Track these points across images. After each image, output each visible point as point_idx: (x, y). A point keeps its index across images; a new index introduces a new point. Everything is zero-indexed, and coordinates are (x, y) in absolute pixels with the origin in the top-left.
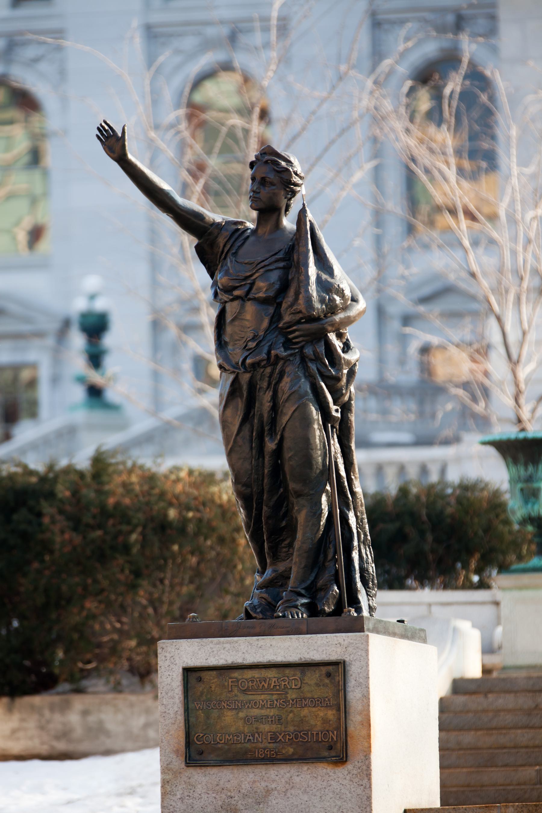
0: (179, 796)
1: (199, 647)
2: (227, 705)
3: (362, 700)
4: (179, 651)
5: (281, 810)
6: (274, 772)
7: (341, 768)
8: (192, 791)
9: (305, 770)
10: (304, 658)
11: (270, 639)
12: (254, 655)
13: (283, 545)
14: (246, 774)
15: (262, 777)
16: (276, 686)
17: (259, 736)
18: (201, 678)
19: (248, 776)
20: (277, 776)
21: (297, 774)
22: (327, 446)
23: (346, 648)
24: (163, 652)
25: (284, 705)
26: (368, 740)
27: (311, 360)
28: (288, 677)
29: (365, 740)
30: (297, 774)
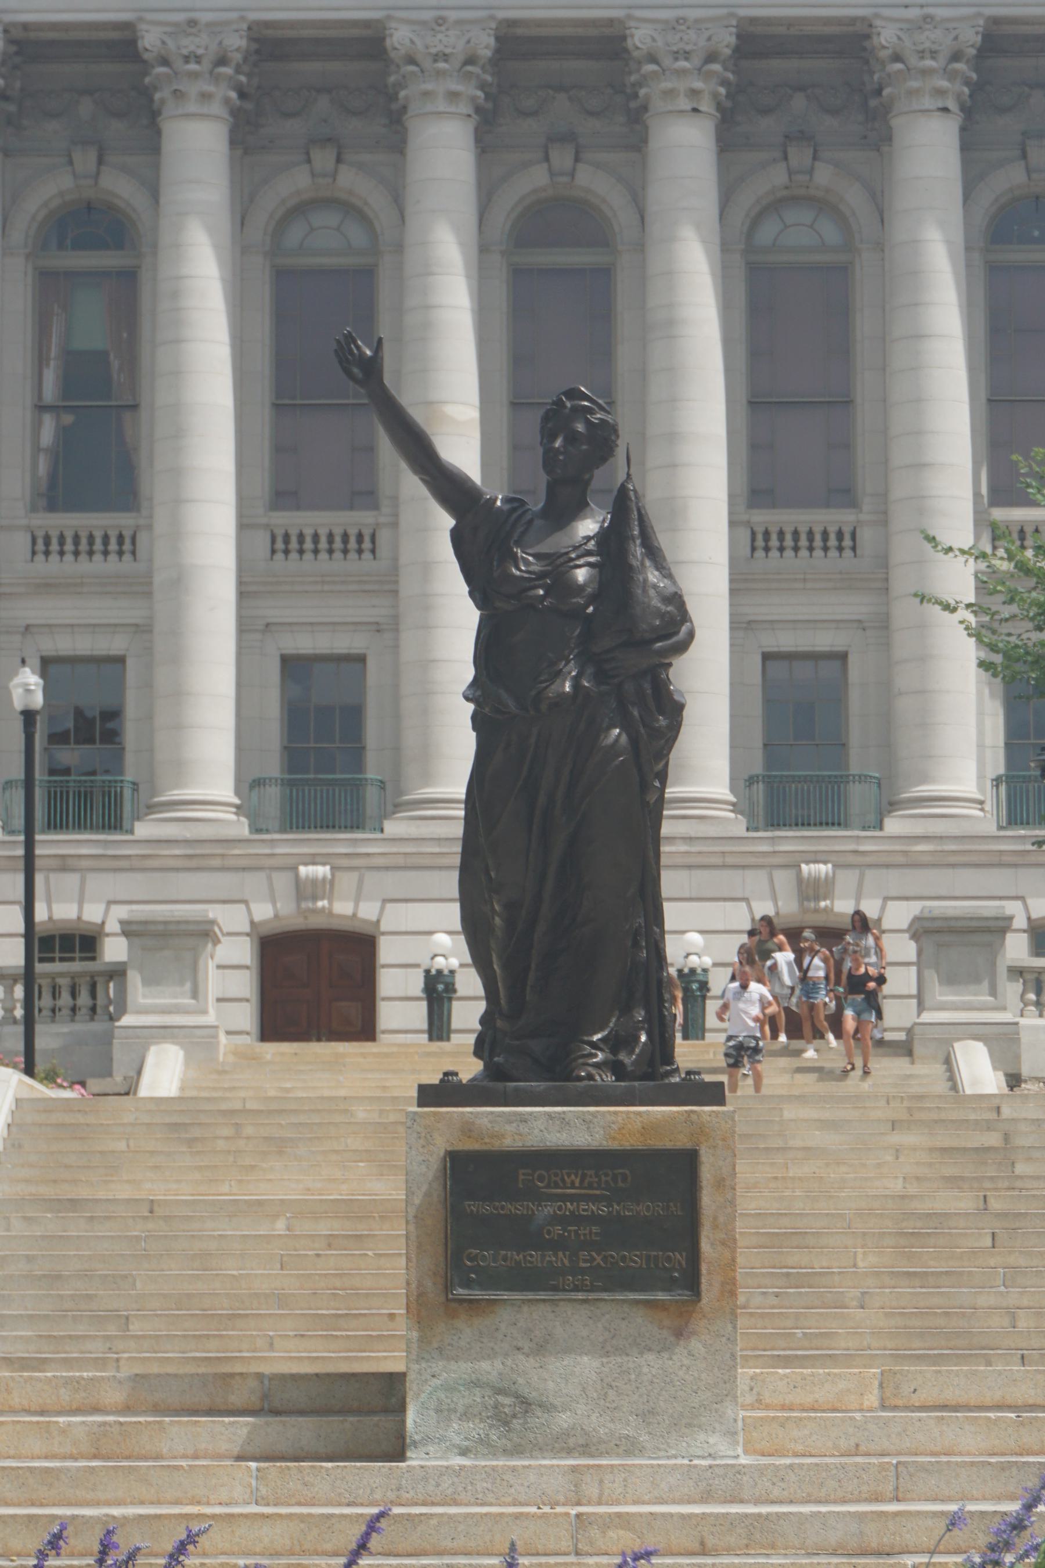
0: (435, 1345)
5: (596, 1370)
8: (455, 1338)
9: (696, 1117)
17: (562, 1260)
22: (501, 989)
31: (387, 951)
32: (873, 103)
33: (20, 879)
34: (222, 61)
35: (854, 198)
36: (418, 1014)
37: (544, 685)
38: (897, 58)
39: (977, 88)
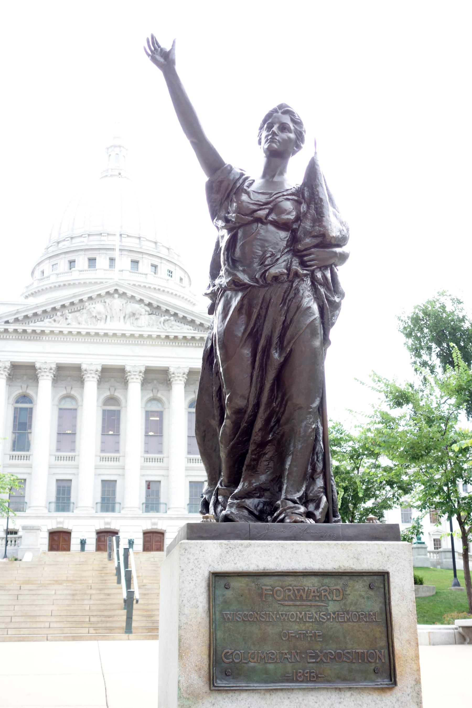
1: (227, 550)
2: (320, 616)
3: (408, 616)
4: (204, 553)
6: (313, 697)
7: (389, 694)
10: (344, 566)
11: (329, 544)
12: (289, 561)
13: (264, 459)
14: (280, 700)
15: (299, 704)
16: (315, 596)
18: (227, 588)
19: (283, 702)
20: (316, 703)
21: (339, 700)
23: (388, 557)
24: (186, 554)
25: (324, 619)
26: (416, 662)
27: (320, 284)
28: (329, 587)
29: (413, 662)
30: (339, 700)
31: (73, 535)
32: (169, 382)
33: (6, 520)
34: (51, 369)
35: (164, 399)
36: (79, 547)
37: (269, 267)
38: (173, 374)
39: (187, 380)
